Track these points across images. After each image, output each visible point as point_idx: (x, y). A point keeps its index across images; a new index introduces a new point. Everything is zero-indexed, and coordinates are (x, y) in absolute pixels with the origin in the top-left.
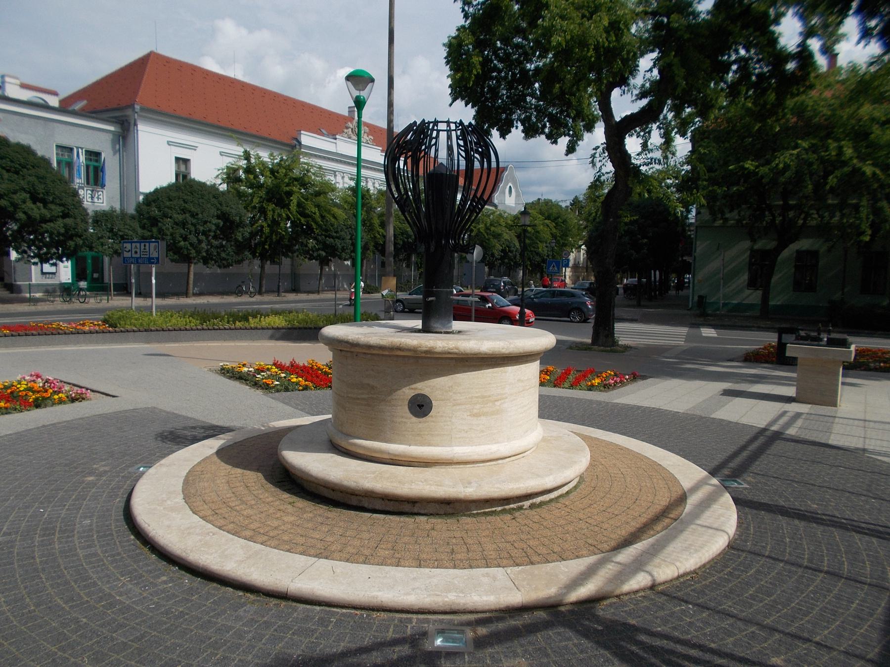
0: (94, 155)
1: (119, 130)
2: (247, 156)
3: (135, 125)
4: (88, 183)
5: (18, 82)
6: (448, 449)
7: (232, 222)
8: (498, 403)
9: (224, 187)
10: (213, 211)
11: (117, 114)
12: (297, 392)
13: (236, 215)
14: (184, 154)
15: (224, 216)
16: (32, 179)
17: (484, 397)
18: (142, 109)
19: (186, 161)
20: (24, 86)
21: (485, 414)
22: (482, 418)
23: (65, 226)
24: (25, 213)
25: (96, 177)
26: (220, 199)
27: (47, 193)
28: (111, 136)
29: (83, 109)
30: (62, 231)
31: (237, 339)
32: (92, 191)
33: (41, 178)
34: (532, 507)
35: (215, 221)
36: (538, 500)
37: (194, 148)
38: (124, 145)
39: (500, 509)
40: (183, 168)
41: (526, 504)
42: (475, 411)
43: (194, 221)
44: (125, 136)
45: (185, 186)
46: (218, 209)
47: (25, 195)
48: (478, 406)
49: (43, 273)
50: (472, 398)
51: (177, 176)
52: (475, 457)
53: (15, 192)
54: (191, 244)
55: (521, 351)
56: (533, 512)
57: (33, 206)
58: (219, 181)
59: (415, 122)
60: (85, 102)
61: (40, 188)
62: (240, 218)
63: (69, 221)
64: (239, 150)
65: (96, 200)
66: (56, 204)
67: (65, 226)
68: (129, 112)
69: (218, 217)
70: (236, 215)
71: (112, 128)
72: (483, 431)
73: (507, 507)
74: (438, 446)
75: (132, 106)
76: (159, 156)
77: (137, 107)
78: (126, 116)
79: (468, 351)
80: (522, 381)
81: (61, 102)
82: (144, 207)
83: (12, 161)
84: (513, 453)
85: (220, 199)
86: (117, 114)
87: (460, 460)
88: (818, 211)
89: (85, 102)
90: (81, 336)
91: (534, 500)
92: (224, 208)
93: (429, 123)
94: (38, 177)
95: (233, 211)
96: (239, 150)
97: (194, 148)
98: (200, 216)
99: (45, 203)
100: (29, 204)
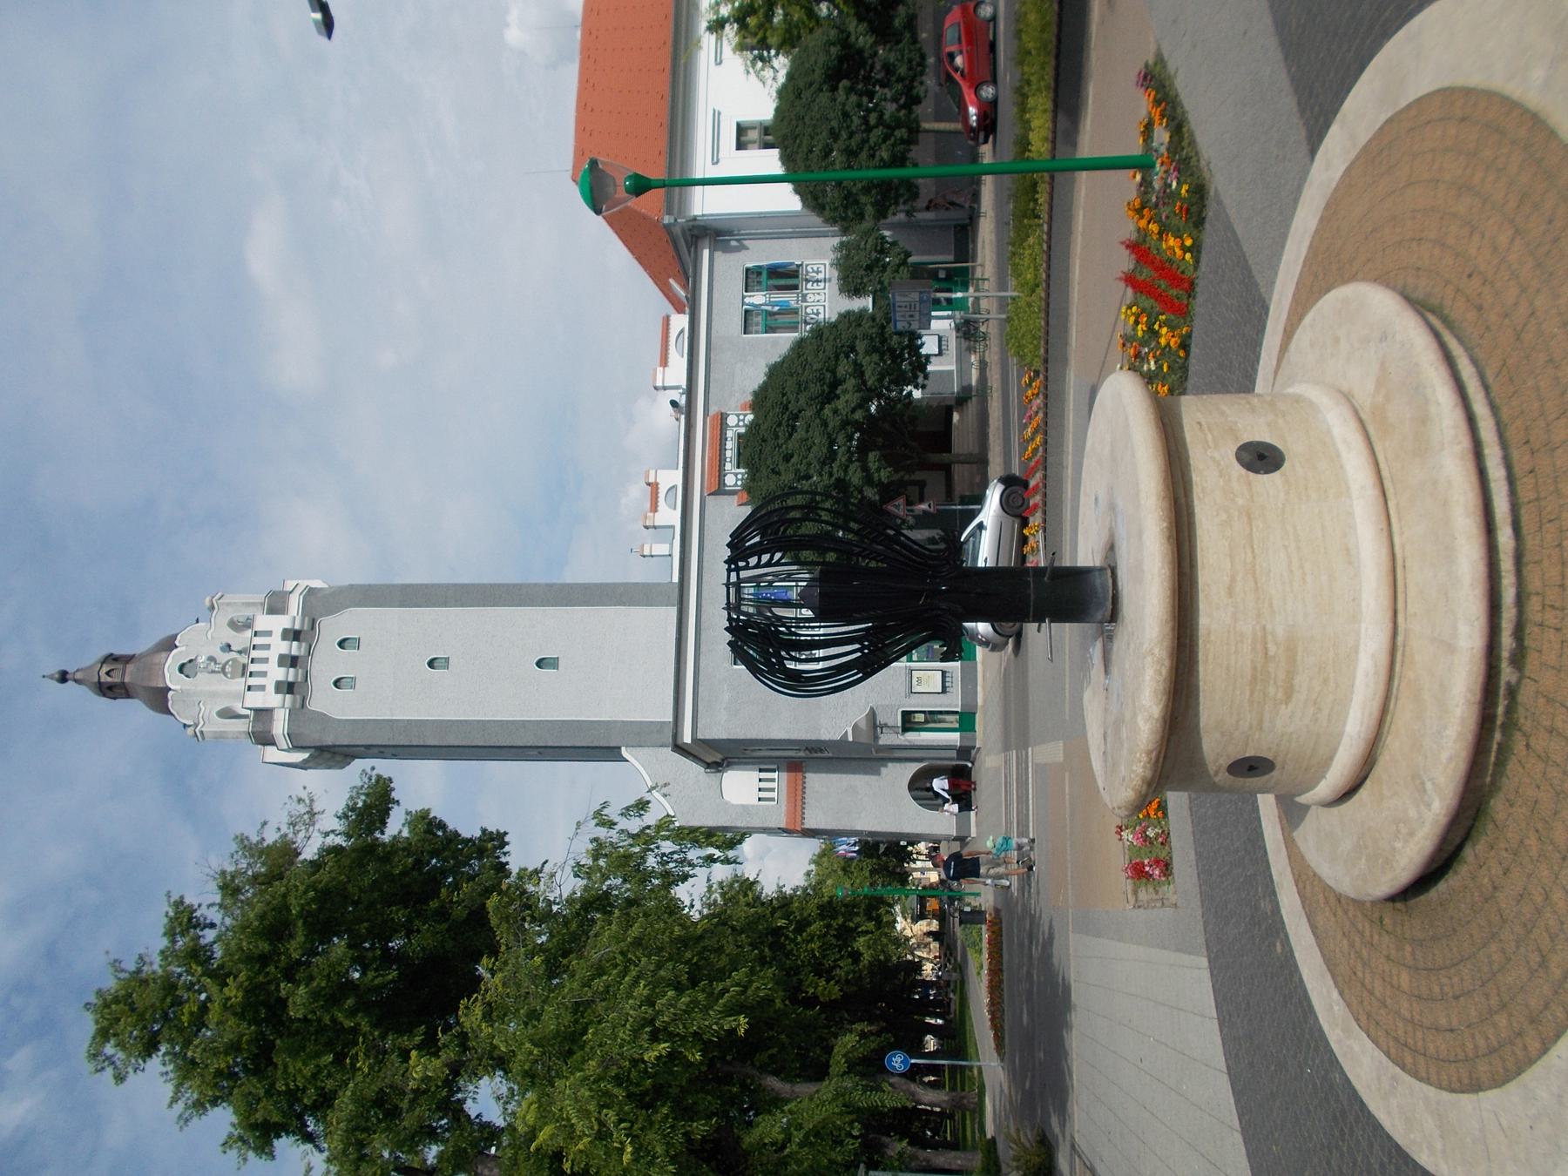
0: (753, 278)
1: (707, 242)
2: (717, 26)
3: (695, 219)
4: (795, 287)
5: (660, 369)
6: (1345, 741)
7: (841, 59)
8: (1272, 649)
9: (782, 64)
10: (824, 98)
11: (684, 249)
12: (1192, 360)
13: (828, 52)
14: (729, 136)
15: (833, 77)
16: (802, 402)
17: (1254, 678)
18: (669, 213)
19: (741, 130)
20: (664, 362)
21: (1291, 674)
22: (1296, 682)
23: (867, 353)
24: (853, 411)
25: (784, 277)
26: (801, 84)
27: (821, 380)
28: (718, 254)
29: (685, 287)
30: (875, 357)
31: (1070, 209)
32: (807, 281)
33: (801, 387)
34: (1518, 659)
35: (841, 94)
36: (1507, 641)
37: (717, 116)
38: (730, 233)
39: (1498, 736)
40: (753, 135)
41: (1507, 674)
42: (1280, 695)
43: (844, 135)
44: (717, 234)
45: (788, 133)
46: (821, 90)
47: (827, 411)
48: (1271, 690)
49: (940, 353)
50: (1251, 702)
51: (767, 146)
52: (1375, 706)
53: (825, 424)
54: (886, 138)
55: (1168, 629)
56: (1532, 662)
57: (843, 399)
58: (768, 73)
59: (730, 644)
60: (671, 281)
61: (815, 389)
62: (834, 44)
63: (861, 346)
64: (708, 41)
65: (821, 276)
66: (836, 365)
67: (867, 353)
68: (677, 231)
69: (834, 89)
70: (828, 52)
71: (706, 253)
72: (1326, 681)
73: (1500, 720)
74: (1335, 750)
75: (667, 227)
76: (738, 177)
77: (667, 220)
78: (683, 232)
79: (1158, 737)
80: (1233, 579)
81: (680, 310)
82: (827, 213)
83: (780, 425)
84: (1389, 615)
85: (801, 84)
86: (684, 249)
87: (1373, 722)
88: (935, 935)
89: (671, 281)
90: (1050, 460)
91: (1505, 654)
92: (818, 75)
93: (730, 619)
94: (799, 391)
95: (822, 59)
96: (708, 41)
97: (717, 116)
98: (834, 124)
99: (836, 383)
100: (840, 404)
